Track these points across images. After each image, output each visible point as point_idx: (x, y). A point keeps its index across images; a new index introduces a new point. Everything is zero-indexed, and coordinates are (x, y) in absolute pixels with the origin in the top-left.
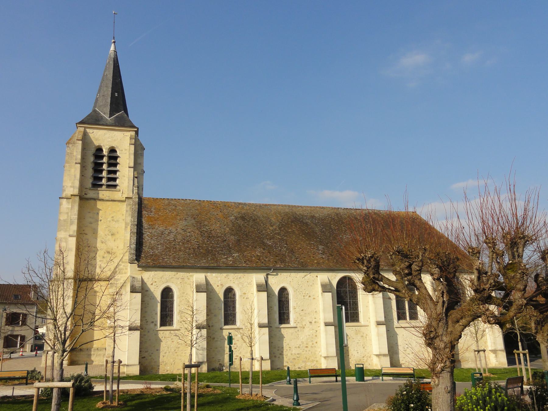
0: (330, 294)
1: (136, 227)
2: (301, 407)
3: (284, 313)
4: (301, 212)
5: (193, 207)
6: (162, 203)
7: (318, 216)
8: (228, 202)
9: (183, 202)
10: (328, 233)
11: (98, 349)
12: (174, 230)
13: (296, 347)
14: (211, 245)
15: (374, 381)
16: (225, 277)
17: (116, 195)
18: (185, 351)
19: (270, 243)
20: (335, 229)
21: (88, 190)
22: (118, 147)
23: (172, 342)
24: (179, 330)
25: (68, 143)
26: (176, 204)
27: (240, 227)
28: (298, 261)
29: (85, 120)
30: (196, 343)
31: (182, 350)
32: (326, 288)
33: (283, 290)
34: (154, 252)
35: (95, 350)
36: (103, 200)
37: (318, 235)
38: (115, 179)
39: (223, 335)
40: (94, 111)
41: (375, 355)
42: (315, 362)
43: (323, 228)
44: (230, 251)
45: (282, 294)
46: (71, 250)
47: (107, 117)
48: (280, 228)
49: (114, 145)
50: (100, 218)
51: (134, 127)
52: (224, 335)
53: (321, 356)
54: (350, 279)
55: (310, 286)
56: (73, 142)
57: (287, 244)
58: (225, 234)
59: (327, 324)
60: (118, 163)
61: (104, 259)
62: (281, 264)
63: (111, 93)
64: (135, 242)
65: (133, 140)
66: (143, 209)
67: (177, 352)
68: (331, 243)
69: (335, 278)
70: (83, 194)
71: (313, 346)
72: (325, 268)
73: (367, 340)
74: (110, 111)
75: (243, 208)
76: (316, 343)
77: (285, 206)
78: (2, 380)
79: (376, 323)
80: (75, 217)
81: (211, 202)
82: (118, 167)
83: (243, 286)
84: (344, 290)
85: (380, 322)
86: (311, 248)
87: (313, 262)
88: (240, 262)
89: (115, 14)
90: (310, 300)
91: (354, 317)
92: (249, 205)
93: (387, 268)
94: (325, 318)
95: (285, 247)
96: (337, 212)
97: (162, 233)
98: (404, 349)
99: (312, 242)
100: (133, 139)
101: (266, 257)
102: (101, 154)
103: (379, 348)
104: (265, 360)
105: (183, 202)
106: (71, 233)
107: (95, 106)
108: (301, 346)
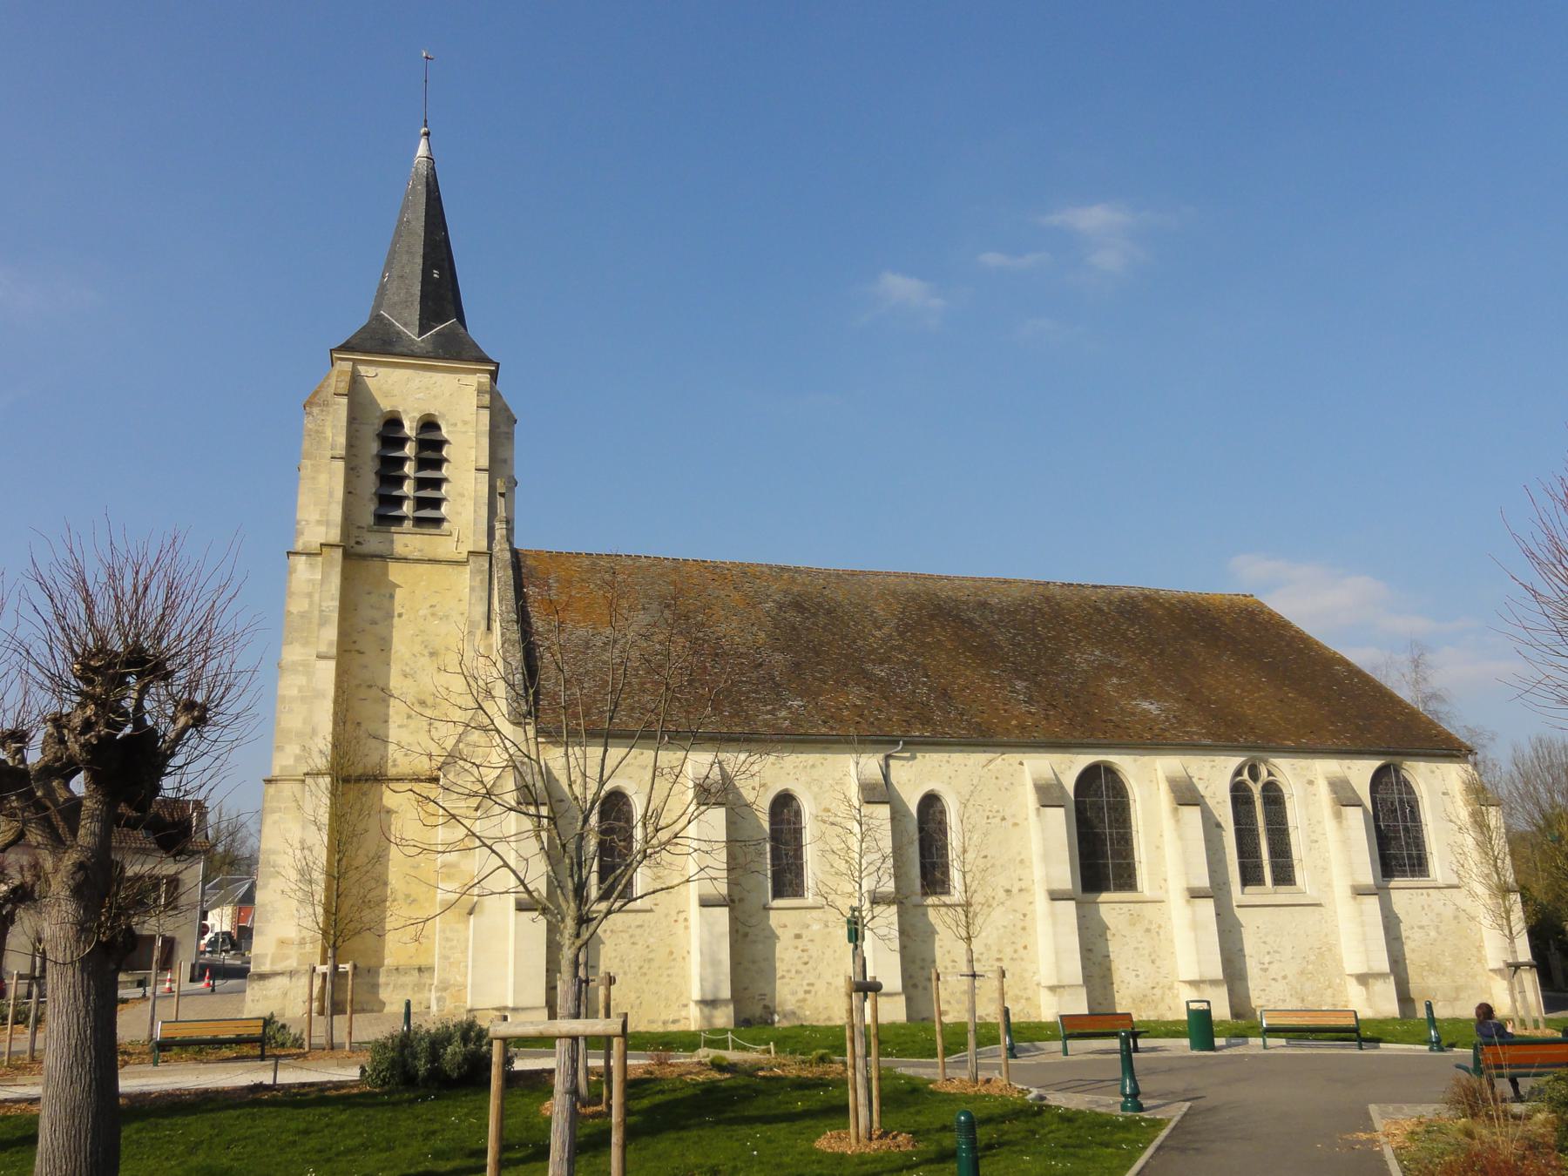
0: (1061, 811)
2: (1145, 1115)
3: (934, 865)
4: (950, 593)
5: (662, 575)
6: (573, 565)
10: (1032, 648)
11: (397, 969)
16: (773, 764)
17: (442, 546)
18: (668, 968)
20: (1048, 638)
24: (651, 911)
27: (794, 629)
28: (966, 720)
30: (873, 918)
31: (659, 968)
32: (1048, 795)
33: (931, 802)
35: (389, 972)
36: (405, 559)
37: (1007, 653)
38: (436, 503)
40: (377, 318)
42: (1023, 1001)
45: (928, 813)
46: (324, 696)
47: (412, 333)
48: (901, 634)
49: (433, 408)
50: (398, 609)
51: (487, 361)
52: (773, 926)
54: (1110, 771)
55: (1003, 789)
56: (321, 402)
57: (927, 677)
59: (1055, 896)
60: (446, 460)
65: (487, 397)
66: (525, 580)
67: (645, 974)
68: (1046, 674)
69: (1069, 767)
70: (352, 543)
71: (1015, 956)
72: (1043, 739)
73: (1160, 940)
75: (793, 580)
76: (1025, 948)
77: (905, 575)
78: (190, 1045)
79: (1186, 893)
80: (332, 604)
82: (445, 471)
83: (821, 788)
85: (1200, 889)
87: (1009, 724)
88: (810, 722)
89: (427, 58)
93: (1209, 742)
95: (924, 684)
96: (1047, 593)
97: (587, 643)
98: (1262, 966)
100: (486, 392)
101: (878, 710)
103: (1199, 962)
105: (630, 562)
106: (323, 649)
107: (378, 306)
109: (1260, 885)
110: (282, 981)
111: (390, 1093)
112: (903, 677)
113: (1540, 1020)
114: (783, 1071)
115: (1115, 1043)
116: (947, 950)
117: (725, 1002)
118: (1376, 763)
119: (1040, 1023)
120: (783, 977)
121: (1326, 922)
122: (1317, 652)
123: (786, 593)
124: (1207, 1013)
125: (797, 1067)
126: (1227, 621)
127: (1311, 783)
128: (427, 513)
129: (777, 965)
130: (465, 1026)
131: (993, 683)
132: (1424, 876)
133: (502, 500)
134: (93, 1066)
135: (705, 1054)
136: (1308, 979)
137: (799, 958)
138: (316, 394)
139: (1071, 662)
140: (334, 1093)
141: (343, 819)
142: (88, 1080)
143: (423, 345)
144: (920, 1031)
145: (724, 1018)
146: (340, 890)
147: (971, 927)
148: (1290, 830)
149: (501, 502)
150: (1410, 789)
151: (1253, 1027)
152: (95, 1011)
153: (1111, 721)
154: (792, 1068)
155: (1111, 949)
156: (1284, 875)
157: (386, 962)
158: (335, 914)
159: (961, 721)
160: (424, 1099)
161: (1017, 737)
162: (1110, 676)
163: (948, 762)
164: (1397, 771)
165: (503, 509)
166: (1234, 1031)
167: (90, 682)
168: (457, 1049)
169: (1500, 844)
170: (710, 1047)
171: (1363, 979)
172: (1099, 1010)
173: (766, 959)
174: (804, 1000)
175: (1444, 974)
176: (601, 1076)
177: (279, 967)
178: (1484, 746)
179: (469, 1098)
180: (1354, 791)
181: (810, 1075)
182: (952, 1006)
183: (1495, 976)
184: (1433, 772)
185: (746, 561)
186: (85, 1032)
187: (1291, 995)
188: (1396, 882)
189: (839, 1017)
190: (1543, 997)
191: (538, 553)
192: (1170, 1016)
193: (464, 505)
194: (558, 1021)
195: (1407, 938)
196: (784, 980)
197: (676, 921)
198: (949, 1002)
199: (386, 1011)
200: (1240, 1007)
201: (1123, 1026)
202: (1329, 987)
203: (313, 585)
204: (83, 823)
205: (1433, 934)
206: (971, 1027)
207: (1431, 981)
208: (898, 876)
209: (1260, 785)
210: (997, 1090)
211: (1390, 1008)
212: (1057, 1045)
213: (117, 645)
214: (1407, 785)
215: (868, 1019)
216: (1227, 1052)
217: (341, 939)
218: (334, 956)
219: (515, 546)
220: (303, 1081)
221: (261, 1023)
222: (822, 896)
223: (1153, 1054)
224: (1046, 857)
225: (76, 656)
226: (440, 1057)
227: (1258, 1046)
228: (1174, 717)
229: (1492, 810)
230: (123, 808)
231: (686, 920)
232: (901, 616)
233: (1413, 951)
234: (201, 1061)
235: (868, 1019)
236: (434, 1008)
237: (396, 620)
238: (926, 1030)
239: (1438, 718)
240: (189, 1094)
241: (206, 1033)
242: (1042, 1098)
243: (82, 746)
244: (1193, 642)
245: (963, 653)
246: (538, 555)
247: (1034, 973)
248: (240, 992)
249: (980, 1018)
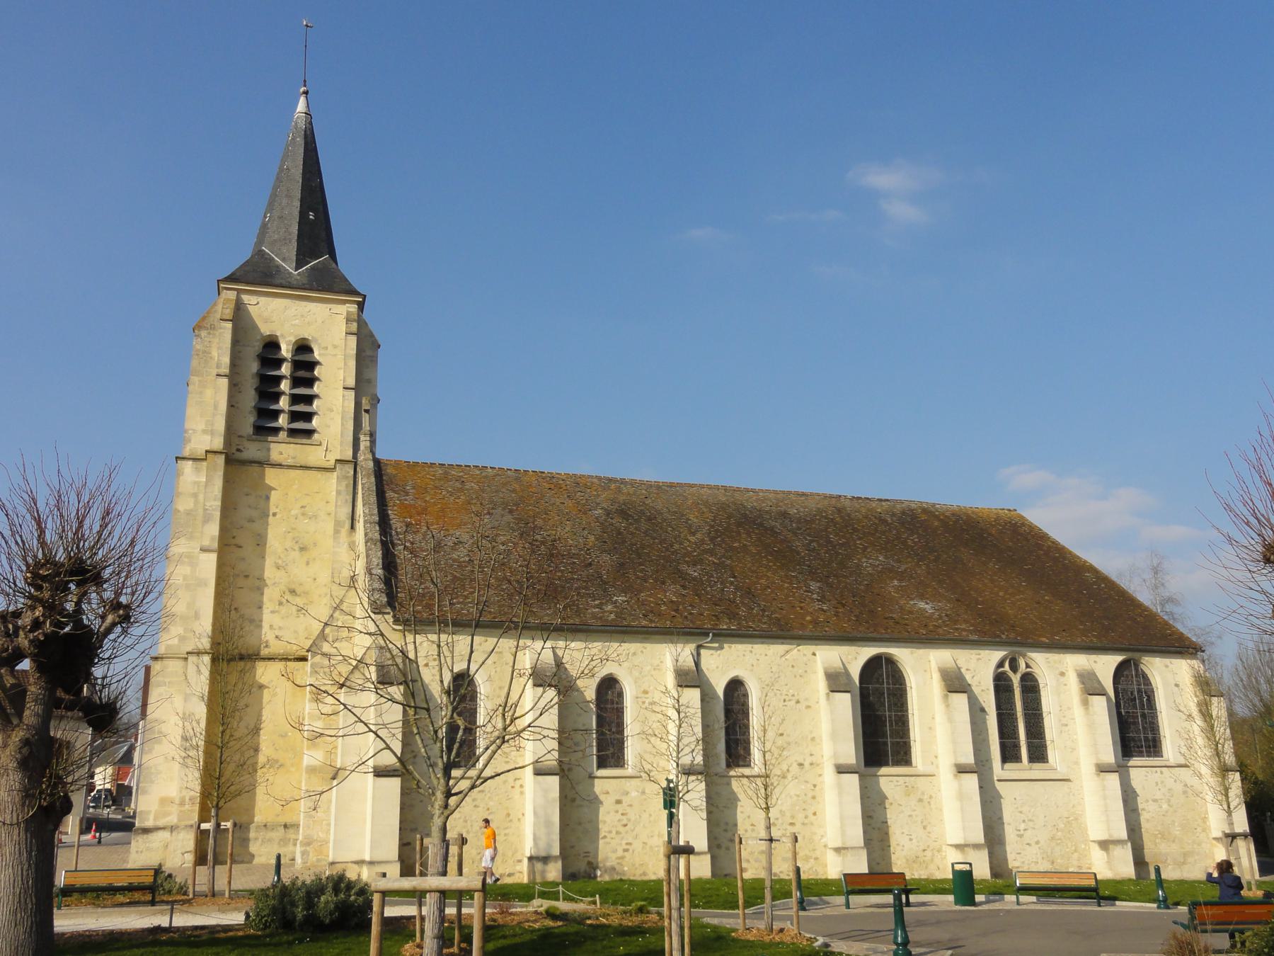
0: (848, 695)
1: (378, 528)
3: (737, 742)
5: (505, 484)
7: (795, 514)
8: (584, 476)
9: (478, 472)
10: (825, 553)
11: (265, 826)
12: (465, 537)
14: (560, 574)
15: (997, 906)
19: (696, 574)
22: (316, 341)
23: (475, 806)
25: (198, 327)
26: (461, 477)
27: (620, 533)
28: (768, 616)
29: (238, 274)
32: (836, 681)
33: (735, 687)
34: (426, 588)
35: (258, 827)
36: (280, 466)
37: (803, 557)
38: (308, 417)
39: (595, 793)
40: (259, 253)
41: (951, 845)
42: (812, 860)
43: (811, 541)
44: (606, 588)
47: (289, 267)
48: (712, 540)
51: (355, 293)
52: (598, 793)
53: (825, 846)
54: (890, 661)
55: (798, 676)
57: (734, 577)
58: (588, 550)
59: (841, 770)
61: (281, 607)
62: (730, 623)
63: (300, 212)
64: (381, 563)
65: (355, 325)
69: (855, 658)
71: (806, 821)
73: (931, 809)
75: (619, 490)
76: (815, 814)
77: (717, 487)
78: (88, 892)
80: (215, 504)
81: (544, 475)
82: (316, 389)
84: (877, 689)
86: (793, 588)
87: (804, 619)
89: (307, 26)
90: (800, 710)
91: (898, 753)
92: (633, 483)
93: (976, 637)
94: (835, 755)
95: (732, 583)
96: (839, 505)
98: (1018, 833)
99: (793, 572)
100: (354, 321)
102: (276, 354)
103: (964, 829)
104: (700, 854)
105: (478, 472)
106: (206, 543)
107: (260, 240)
108: (780, 821)
109: (1017, 762)
110: (164, 835)
111: (271, 935)
112: (712, 576)
113: (1253, 882)
114: (607, 920)
115: (889, 899)
116: (748, 817)
117: (555, 858)
118: (1117, 659)
119: (827, 880)
120: (605, 837)
121: (1074, 795)
122: (1070, 561)
123: (613, 501)
124: (970, 873)
125: (619, 917)
126: (994, 532)
127: (1062, 674)
130: (336, 879)
131: (791, 583)
132: (1158, 757)
133: (367, 415)
134: (34, 910)
135: (539, 904)
136: (1058, 844)
137: (619, 820)
138: (204, 318)
139: (858, 566)
140: (222, 935)
141: (227, 696)
142: (29, 923)
143: (298, 278)
144: (724, 885)
145: (554, 872)
146: (223, 759)
147: (769, 799)
148: (1044, 715)
149: (365, 418)
150: (1147, 681)
151: (1009, 886)
152: (37, 865)
153: (892, 618)
154: (615, 917)
155: (888, 816)
156: (1038, 754)
157: (256, 819)
158: (219, 779)
159: (763, 616)
160: (301, 941)
161: (811, 631)
162: (892, 579)
163: (751, 652)
164: (1137, 666)
165: (368, 424)
166: (993, 889)
167: (39, 588)
168: (330, 898)
169: (1222, 731)
170: (543, 898)
171: (1104, 845)
172: (879, 869)
173: (590, 822)
174: (622, 858)
175: (1174, 841)
176: (452, 923)
177: (160, 823)
178: (1212, 643)
179: (339, 941)
180: (1099, 682)
181: (630, 924)
182: (752, 867)
183: (1218, 844)
184: (1167, 666)
185: (578, 473)
186: (28, 882)
187: (1043, 858)
188: (1135, 761)
189: (654, 868)
190: (1259, 862)
191: (397, 463)
192: (939, 875)
193: (332, 419)
194: (429, 878)
195: (1143, 809)
196: (606, 840)
197: (513, 787)
198: (748, 861)
199: (254, 862)
200: (999, 868)
201: (897, 883)
202: (1076, 851)
203: (198, 486)
204: (28, 706)
205: (1165, 806)
206: (768, 884)
207: (1163, 848)
208: (707, 755)
209: (1019, 675)
210: (789, 938)
211: (1126, 869)
212: (840, 900)
213: (61, 556)
214: (1145, 677)
215: (682, 875)
216: (985, 907)
217: (223, 801)
218: (217, 815)
219: (377, 456)
220: (196, 924)
221: (152, 873)
222: (646, 772)
223: (922, 909)
224: (834, 736)
225: (28, 565)
226: (314, 905)
227: (1013, 902)
228: (947, 615)
229: (1215, 700)
230: (60, 693)
231: (521, 786)
232: (713, 523)
233: (1148, 820)
234: (99, 906)
235: (682, 875)
236: (299, 860)
237: (271, 518)
238: (727, 884)
239: (1174, 619)
240: (98, 935)
241: (102, 881)
242: (826, 945)
243: (31, 642)
244: (963, 549)
245: (765, 557)
246: (397, 464)
247: (822, 836)
248: (125, 844)
249: (775, 875)
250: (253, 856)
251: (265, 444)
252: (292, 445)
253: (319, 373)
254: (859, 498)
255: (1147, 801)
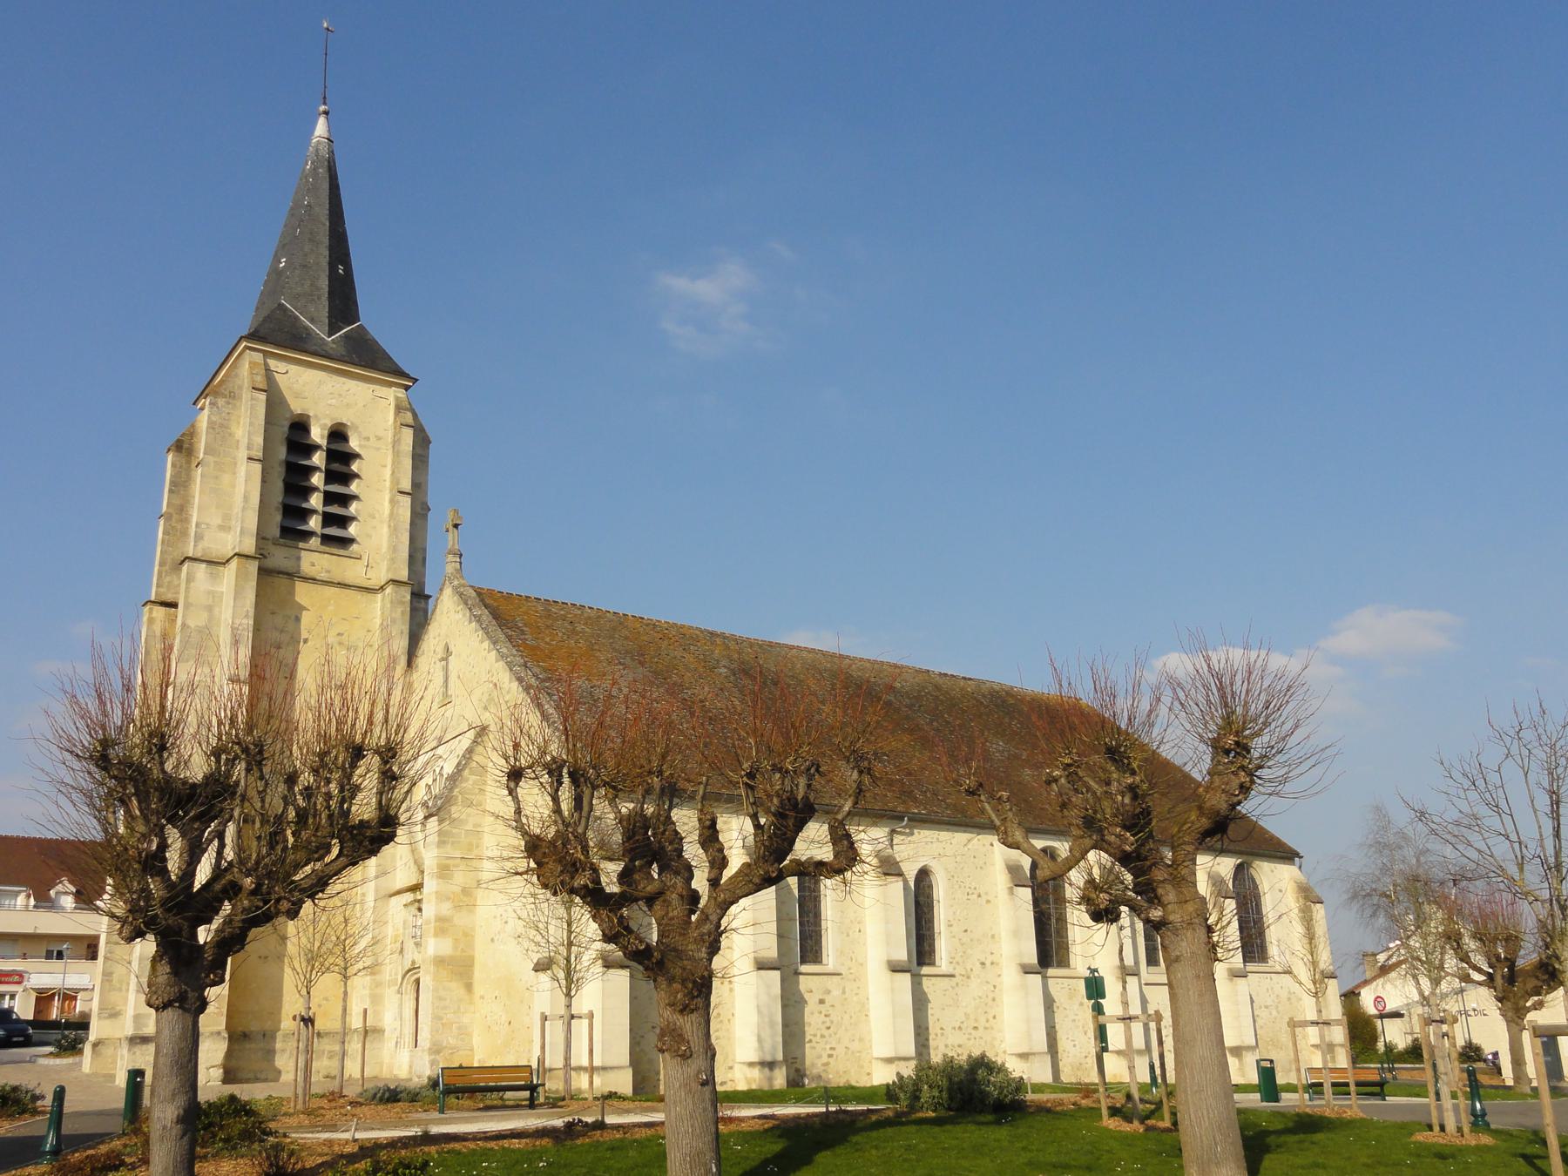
13: (954, 1028)
17: (352, 571)
21: (270, 542)
22: (356, 428)
35: (286, 1036)
36: (314, 580)
38: (343, 521)
39: (800, 991)
47: (319, 331)
50: (304, 635)
52: (803, 991)
63: (330, 263)
71: (987, 1025)
74: (330, 317)
76: (994, 1017)
120: (810, 1041)
128: (333, 531)
129: (806, 1028)
137: (823, 1023)
145: (780, 1080)
157: (282, 1026)
174: (827, 1064)
199: (281, 1080)
203: (213, 597)
205: (1274, 1013)
224: (1016, 933)
250: (280, 1072)
251: (294, 551)
252: (326, 555)
253: (359, 469)
254: (946, 675)
255: (1260, 1007)
